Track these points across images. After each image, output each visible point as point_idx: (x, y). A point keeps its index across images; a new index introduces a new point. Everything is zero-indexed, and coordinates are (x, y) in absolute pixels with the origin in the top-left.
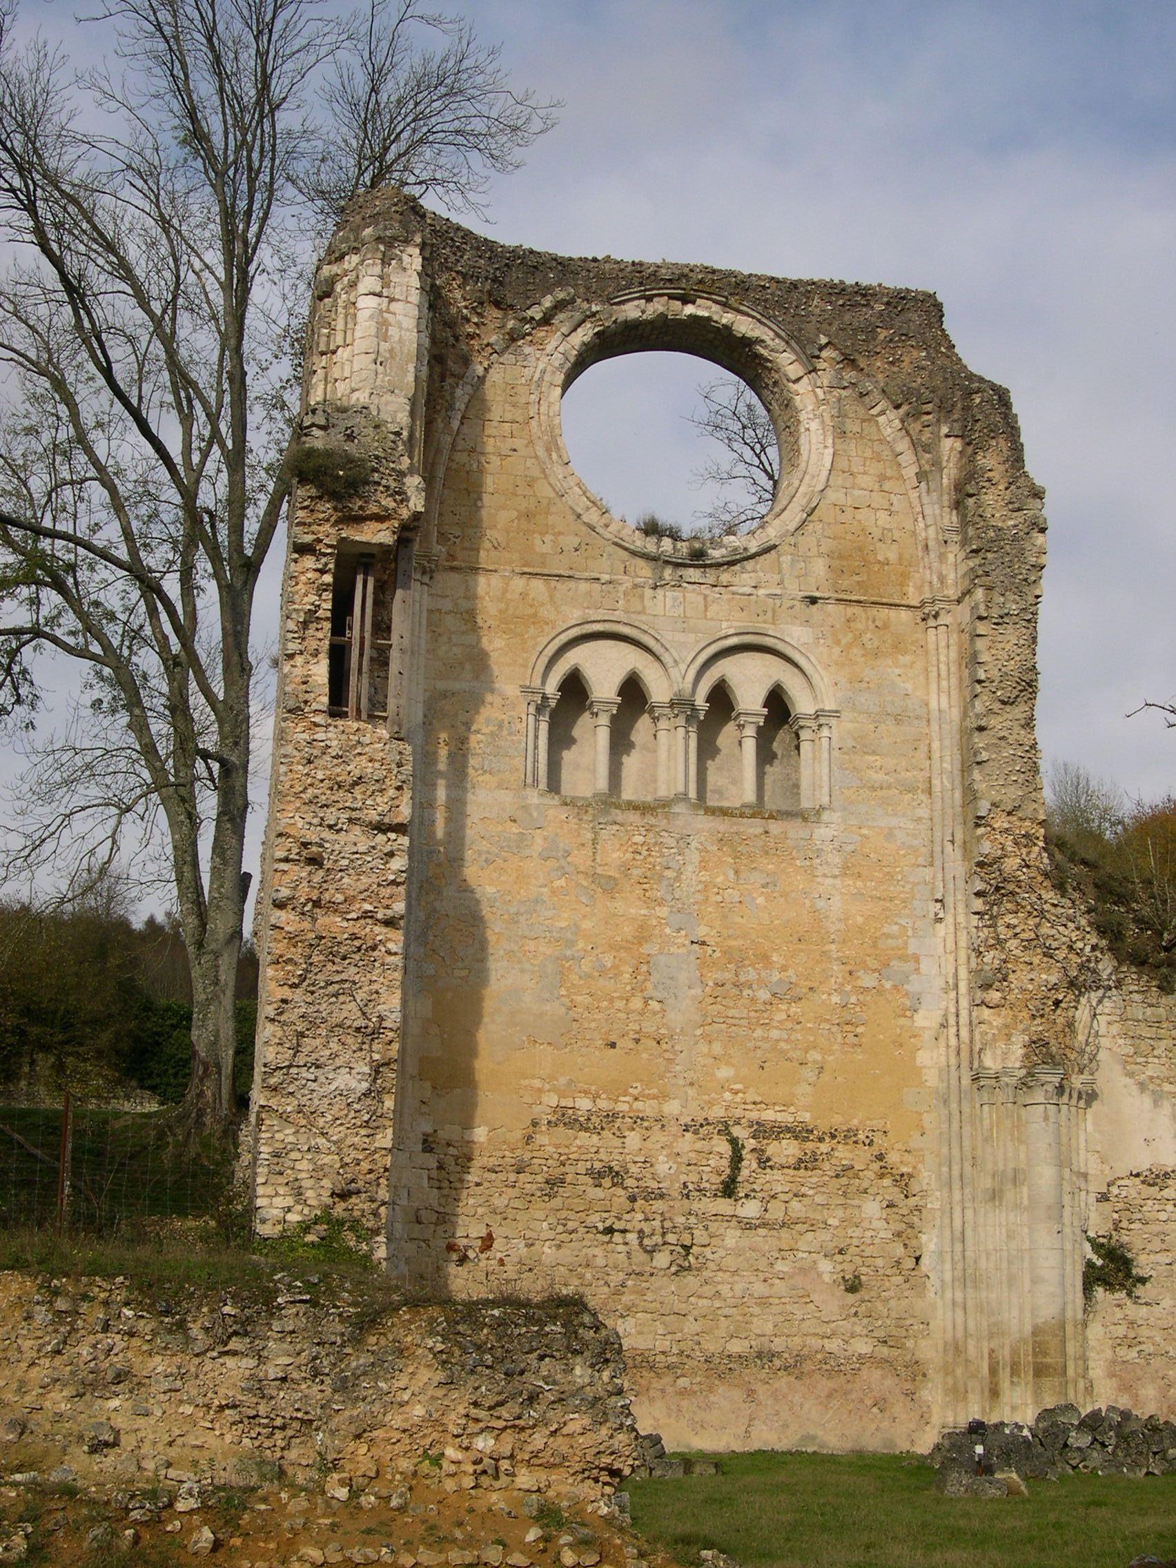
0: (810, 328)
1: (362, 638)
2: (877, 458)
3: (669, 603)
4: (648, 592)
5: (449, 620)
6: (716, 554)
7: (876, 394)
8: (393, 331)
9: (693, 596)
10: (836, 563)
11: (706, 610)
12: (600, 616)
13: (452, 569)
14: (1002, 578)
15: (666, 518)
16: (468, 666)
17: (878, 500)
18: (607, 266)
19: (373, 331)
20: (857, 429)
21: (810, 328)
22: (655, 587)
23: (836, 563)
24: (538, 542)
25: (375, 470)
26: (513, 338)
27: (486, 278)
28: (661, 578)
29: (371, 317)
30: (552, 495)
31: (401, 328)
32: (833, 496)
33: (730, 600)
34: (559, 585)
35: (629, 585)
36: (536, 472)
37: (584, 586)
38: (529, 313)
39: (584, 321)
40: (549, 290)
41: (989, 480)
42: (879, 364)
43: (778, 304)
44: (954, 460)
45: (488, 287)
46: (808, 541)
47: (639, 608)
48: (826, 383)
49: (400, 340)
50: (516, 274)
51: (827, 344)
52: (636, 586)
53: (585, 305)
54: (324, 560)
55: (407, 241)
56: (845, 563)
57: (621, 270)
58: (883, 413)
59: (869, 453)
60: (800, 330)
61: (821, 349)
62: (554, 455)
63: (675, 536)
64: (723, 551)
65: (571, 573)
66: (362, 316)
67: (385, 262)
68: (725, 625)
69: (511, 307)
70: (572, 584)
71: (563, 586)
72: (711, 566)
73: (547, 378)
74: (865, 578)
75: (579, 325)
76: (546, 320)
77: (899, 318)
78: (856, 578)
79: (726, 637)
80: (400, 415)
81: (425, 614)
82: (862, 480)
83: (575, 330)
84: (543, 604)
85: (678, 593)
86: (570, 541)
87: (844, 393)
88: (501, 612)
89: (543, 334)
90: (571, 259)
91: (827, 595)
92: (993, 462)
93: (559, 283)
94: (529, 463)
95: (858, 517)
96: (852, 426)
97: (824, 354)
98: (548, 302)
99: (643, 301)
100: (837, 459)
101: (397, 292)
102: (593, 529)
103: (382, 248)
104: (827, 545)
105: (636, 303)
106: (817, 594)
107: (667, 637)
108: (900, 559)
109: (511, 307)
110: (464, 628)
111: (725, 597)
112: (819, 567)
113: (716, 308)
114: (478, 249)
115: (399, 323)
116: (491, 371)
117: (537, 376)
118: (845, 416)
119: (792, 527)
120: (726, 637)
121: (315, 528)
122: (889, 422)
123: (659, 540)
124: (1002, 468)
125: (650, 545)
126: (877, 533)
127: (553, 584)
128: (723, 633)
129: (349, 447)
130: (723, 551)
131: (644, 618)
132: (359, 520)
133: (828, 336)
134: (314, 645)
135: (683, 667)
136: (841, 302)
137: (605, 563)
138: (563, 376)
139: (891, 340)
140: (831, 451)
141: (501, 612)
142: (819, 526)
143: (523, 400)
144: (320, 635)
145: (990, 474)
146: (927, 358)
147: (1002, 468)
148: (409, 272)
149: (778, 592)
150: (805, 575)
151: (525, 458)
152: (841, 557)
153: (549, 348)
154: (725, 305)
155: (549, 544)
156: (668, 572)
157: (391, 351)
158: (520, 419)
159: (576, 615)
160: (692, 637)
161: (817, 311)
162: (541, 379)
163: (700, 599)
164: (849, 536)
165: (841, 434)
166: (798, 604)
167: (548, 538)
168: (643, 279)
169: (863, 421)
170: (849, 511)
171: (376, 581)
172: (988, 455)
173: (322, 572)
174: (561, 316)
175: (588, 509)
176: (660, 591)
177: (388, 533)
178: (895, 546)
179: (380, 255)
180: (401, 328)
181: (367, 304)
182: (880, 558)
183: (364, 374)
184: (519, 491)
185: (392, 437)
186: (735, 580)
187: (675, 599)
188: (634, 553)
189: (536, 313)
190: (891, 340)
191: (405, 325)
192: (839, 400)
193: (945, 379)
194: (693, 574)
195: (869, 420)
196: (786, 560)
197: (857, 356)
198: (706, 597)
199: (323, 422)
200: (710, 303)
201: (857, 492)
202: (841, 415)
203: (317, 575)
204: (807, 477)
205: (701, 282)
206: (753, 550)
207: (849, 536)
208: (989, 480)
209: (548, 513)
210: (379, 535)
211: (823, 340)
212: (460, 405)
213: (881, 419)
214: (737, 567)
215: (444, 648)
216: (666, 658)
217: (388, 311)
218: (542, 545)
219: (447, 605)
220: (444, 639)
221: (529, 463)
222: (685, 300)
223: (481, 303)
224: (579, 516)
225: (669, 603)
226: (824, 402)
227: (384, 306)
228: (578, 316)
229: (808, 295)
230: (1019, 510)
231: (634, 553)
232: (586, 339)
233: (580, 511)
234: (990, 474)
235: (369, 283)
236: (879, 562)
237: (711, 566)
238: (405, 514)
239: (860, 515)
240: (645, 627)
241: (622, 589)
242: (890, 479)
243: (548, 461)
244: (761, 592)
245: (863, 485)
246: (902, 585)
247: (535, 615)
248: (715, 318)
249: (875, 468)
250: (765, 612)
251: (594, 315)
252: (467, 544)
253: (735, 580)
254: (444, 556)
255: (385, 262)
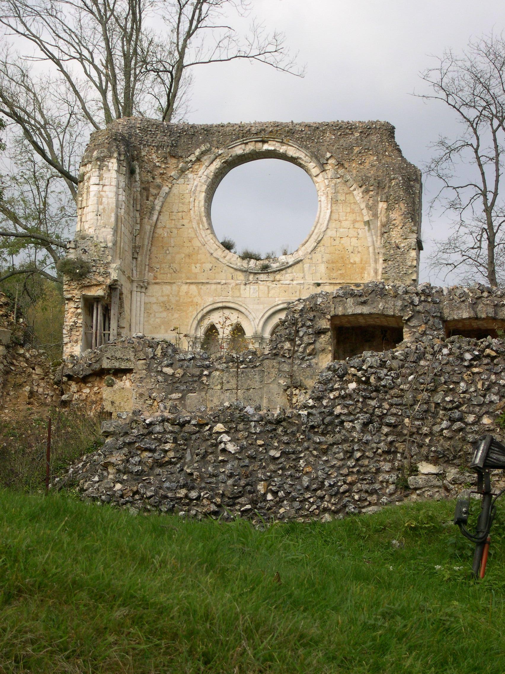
0: (323, 148)
1: (96, 332)
2: (353, 212)
3: (252, 291)
4: (243, 287)
5: (155, 307)
6: (275, 266)
7: (351, 182)
8: (104, 200)
9: (262, 287)
10: (330, 266)
11: (268, 293)
12: (220, 300)
13: (156, 283)
14: (393, 274)
15: (253, 249)
16: (163, 327)
17: (352, 232)
18: (228, 129)
19: (95, 202)
20: (343, 198)
21: (323, 148)
22: (246, 284)
23: (330, 266)
24: (193, 267)
25: (93, 266)
26: (183, 171)
27: (168, 146)
28: (248, 280)
29: (95, 195)
30: (200, 245)
31: (108, 198)
32: (330, 233)
33: (280, 287)
34: (202, 287)
35: (234, 284)
36: (193, 235)
37: (213, 287)
38: (190, 158)
39: (216, 158)
40: (198, 146)
41: (394, 225)
42: (354, 165)
43: (309, 138)
44: (383, 213)
45: (168, 150)
46: (317, 256)
47: (238, 295)
48: (329, 177)
49: (108, 204)
50: (184, 140)
51: (330, 157)
52: (237, 285)
53: (216, 150)
54: (77, 304)
55: (111, 157)
56: (334, 265)
57: (234, 130)
58: (355, 190)
59: (348, 210)
60: (318, 150)
61: (327, 159)
62: (201, 226)
63: (258, 259)
64: (278, 264)
65: (207, 281)
66: (92, 194)
67: (100, 168)
68: (277, 299)
69: (181, 157)
70: (208, 286)
71: (204, 287)
72: (271, 272)
73: (198, 189)
74: (344, 271)
75: (214, 160)
76: (198, 159)
77: (366, 140)
78: (340, 272)
79: (278, 305)
80: (108, 236)
81: (143, 306)
82: (346, 224)
83: (212, 163)
84: (195, 296)
85: (256, 286)
86: (208, 266)
87: (338, 180)
88: (177, 301)
89: (197, 167)
90: (212, 126)
91: (325, 282)
92: (397, 215)
93: (203, 142)
94: (190, 231)
95: (342, 242)
96: (341, 197)
97: (330, 161)
98: (197, 152)
99: (243, 145)
100: (333, 214)
101: (106, 182)
102: (218, 259)
103: (99, 163)
104: (327, 257)
105: (240, 146)
106: (320, 282)
107: (251, 307)
108: (361, 260)
109: (181, 157)
110: (161, 310)
111: (278, 286)
112: (322, 268)
113: (278, 144)
114: (164, 132)
115: (107, 196)
116: (173, 188)
117: (193, 189)
118: (338, 192)
119: (309, 251)
120: (278, 305)
121: (71, 292)
122: (358, 194)
123: (249, 262)
124: (400, 218)
125: (244, 264)
126: (350, 249)
127: (200, 286)
128: (276, 303)
129: (84, 257)
130: (278, 264)
131: (240, 299)
132: (89, 286)
133: (331, 153)
134: (75, 338)
135: (257, 321)
136: (339, 134)
137: (223, 275)
138: (206, 186)
139: (360, 153)
140: (329, 211)
141: (177, 301)
142: (322, 248)
143: (187, 201)
144: (78, 334)
145: (394, 222)
146: (377, 160)
147: (400, 218)
148: (111, 171)
149: (302, 282)
150: (316, 272)
151: (188, 229)
152: (333, 262)
153: (200, 173)
154: (282, 143)
155: (198, 268)
156: (251, 277)
157: (104, 209)
158: (186, 210)
159: (210, 300)
160: (261, 306)
161: (328, 139)
162: (195, 190)
163: (266, 288)
164: (337, 252)
165: (334, 201)
166: (311, 287)
167: (198, 265)
168: (243, 133)
169: (347, 194)
170: (338, 240)
171: (103, 306)
172: (394, 212)
173: (77, 308)
174: (205, 157)
175: (216, 250)
176: (248, 286)
177: (101, 291)
178: (359, 255)
179: (97, 167)
180: (108, 198)
181: (94, 189)
182: (352, 261)
183: (92, 221)
184: (185, 244)
185: (102, 249)
186: (283, 278)
187: (254, 289)
188: (236, 270)
189: (193, 158)
190: (360, 153)
191: (110, 196)
192: (336, 184)
193: (383, 171)
194: (263, 277)
195: (349, 193)
196: (306, 266)
197: (344, 162)
198: (268, 287)
199: (73, 246)
200: (274, 143)
201: (342, 230)
202: (336, 192)
203: (75, 310)
204: (319, 225)
205: (271, 132)
206: (290, 264)
207: (337, 252)
208: (394, 225)
209: (198, 254)
210: (98, 292)
211: (328, 155)
212: (158, 208)
213: (355, 192)
214: (284, 272)
215: (152, 319)
216: (250, 317)
217: (102, 191)
218: (195, 269)
219: (153, 300)
220: (153, 315)
221: (190, 231)
222: (264, 142)
223: (166, 158)
224: (212, 254)
225: (252, 291)
226: (328, 186)
227: (101, 189)
228: (212, 156)
229: (324, 132)
230: (406, 239)
231: (236, 270)
232: (218, 167)
233: (212, 252)
234: (394, 222)
235: (94, 180)
236: (351, 263)
237: (271, 272)
238: (108, 282)
239: (343, 241)
240: (240, 303)
241: (230, 286)
242: (358, 221)
243: (198, 229)
244: (295, 282)
245: (345, 226)
246: (361, 273)
247: (192, 301)
248: (278, 149)
249: (351, 217)
250: (296, 292)
251: (220, 155)
252: (162, 272)
253: (283, 278)
254: (152, 278)
255: (100, 168)
